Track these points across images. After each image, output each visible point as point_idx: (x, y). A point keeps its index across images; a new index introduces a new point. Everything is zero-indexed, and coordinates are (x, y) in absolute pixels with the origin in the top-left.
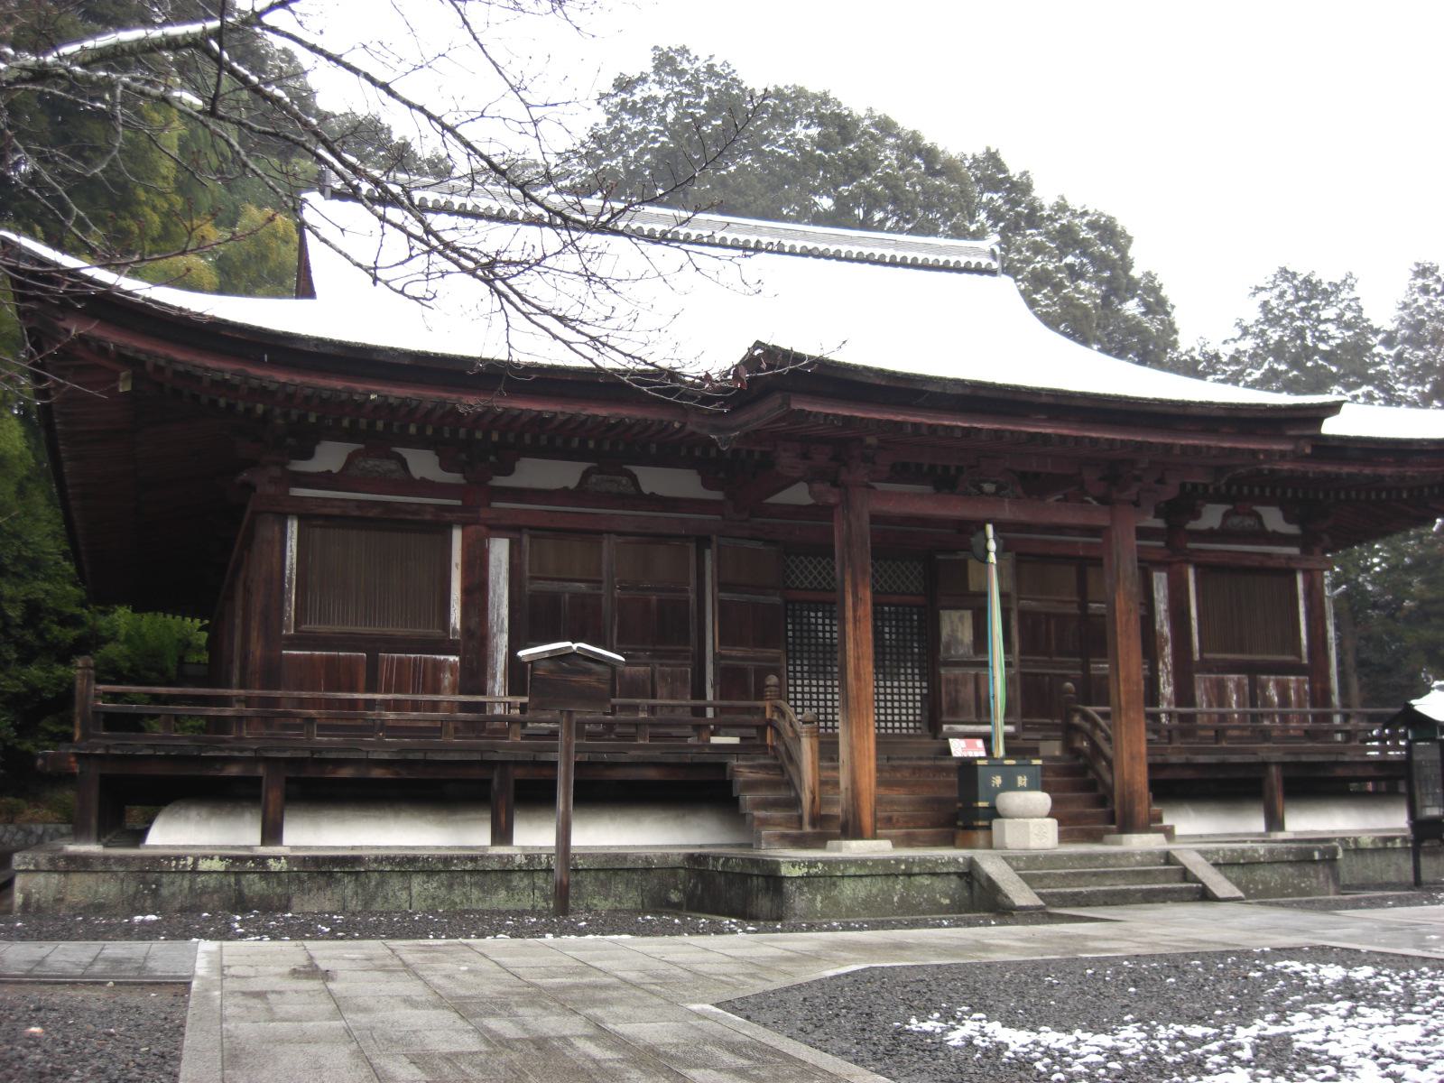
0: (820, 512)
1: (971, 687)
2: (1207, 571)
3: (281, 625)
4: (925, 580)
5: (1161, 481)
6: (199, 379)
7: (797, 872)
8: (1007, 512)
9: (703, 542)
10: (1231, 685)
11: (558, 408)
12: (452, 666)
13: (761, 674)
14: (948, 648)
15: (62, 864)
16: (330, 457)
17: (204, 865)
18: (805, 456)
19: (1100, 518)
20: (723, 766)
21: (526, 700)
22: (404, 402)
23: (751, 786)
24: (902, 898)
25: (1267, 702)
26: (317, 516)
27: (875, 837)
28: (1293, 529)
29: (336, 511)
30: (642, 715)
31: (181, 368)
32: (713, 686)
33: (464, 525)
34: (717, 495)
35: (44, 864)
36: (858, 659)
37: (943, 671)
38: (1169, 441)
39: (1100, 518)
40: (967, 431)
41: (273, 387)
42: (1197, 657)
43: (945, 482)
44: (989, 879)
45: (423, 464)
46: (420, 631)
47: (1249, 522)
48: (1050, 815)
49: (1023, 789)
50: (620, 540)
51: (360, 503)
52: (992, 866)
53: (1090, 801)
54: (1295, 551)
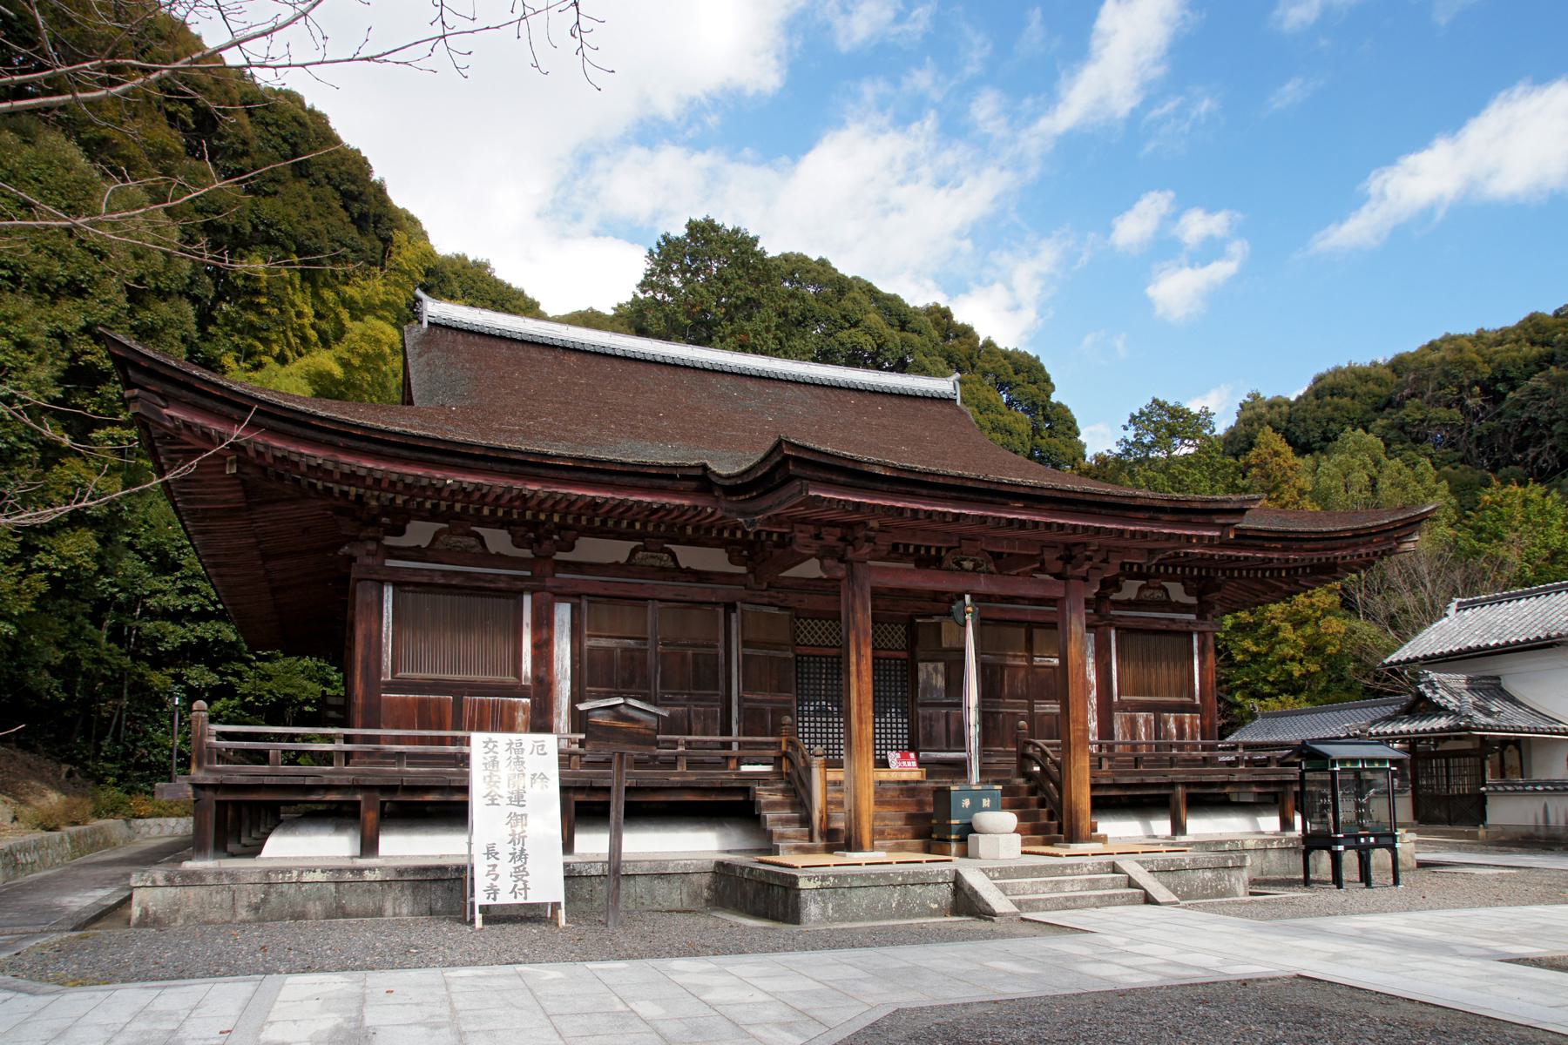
0: (827, 587)
1: (943, 722)
2: (1124, 632)
3: (379, 674)
4: (912, 637)
5: (1105, 561)
6: (296, 464)
7: (812, 885)
8: (983, 585)
9: (730, 607)
10: (1141, 721)
11: (609, 495)
12: (524, 707)
13: (778, 713)
14: (925, 690)
15: (178, 880)
16: (419, 533)
17: (307, 877)
18: (818, 537)
19: (1058, 591)
20: (746, 790)
21: (583, 736)
22: (478, 487)
23: (772, 805)
24: (899, 904)
25: (1168, 734)
26: (408, 584)
27: (873, 848)
28: (1193, 600)
29: (425, 580)
30: (681, 749)
31: (279, 454)
32: (738, 723)
33: (533, 592)
34: (742, 570)
35: (160, 880)
36: (860, 705)
37: (920, 711)
38: (1121, 527)
39: (1058, 591)
40: (957, 517)
41: (362, 472)
42: (1116, 699)
43: (929, 561)
44: (971, 888)
45: (498, 540)
46: (498, 678)
47: (1159, 594)
48: (1016, 831)
49: (986, 809)
50: (662, 605)
51: (444, 573)
52: (975, 878)
53: (1049, 820)
54: (1193, 617)
